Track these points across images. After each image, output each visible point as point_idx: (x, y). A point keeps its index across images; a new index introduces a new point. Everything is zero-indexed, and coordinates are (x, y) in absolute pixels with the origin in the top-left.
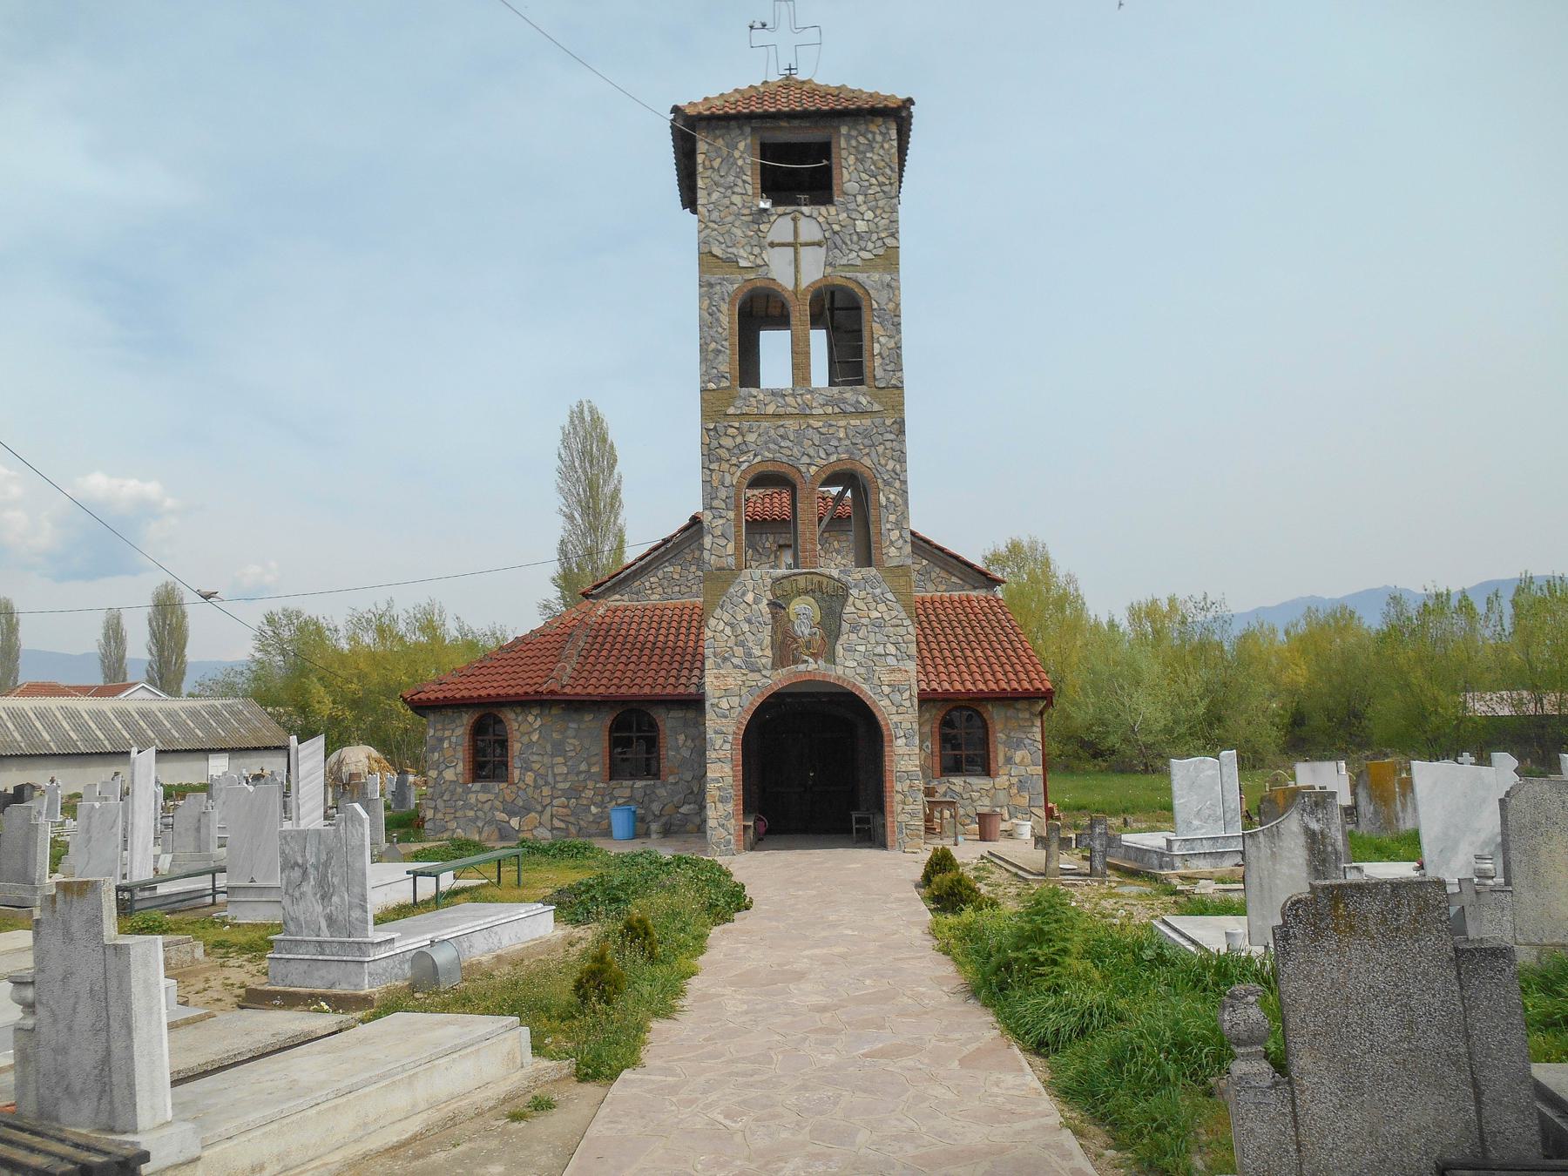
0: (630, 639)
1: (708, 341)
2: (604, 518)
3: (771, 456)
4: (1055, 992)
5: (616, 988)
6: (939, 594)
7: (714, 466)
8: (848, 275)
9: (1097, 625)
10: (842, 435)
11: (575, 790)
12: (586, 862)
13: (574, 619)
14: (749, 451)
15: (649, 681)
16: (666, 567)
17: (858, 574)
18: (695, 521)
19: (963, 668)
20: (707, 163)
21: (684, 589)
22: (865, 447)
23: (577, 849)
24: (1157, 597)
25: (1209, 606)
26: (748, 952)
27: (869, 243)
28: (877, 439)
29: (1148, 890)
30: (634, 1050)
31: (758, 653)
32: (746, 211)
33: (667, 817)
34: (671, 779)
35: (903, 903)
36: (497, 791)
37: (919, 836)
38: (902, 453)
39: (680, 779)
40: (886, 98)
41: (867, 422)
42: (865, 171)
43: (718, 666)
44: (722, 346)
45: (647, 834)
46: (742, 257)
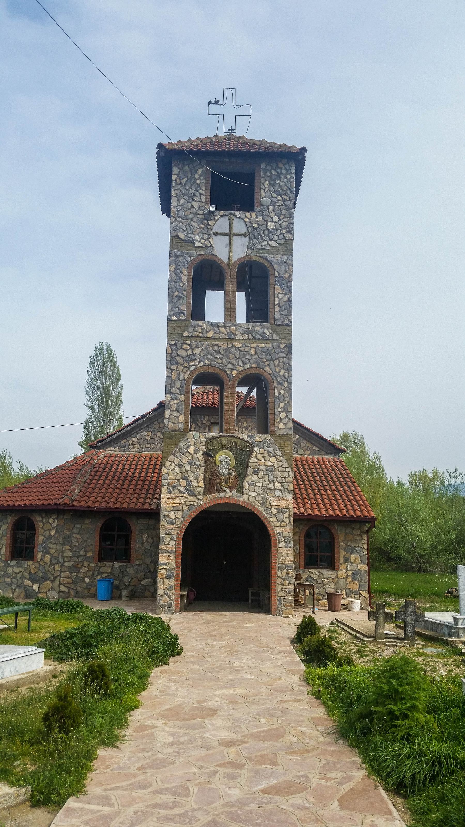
0: (118, 474)
1: (174, 291)
2: (112, 409)
3: (209, 363)
4: (408, 741)
5: (74, 721)
6: (306, 456)
7: (174, 367)
8: (262, 255)
9: (391, 483)
10: (253, 352)
11: (76, 567)
12: (77, 616)
13: (84, 461)
14: (196, 359)
15: (127, 500)
16: (142, 432)
17: (259, 438)
18: (161, 405)
19: (320, 501)
20: (178, 180)
21: (152, 446)
22: (267, 360)
23: (72, 606)
24: (426, 469)
25: (458, 476)
26: (177, 689)
27: (275, 236)
28: (275, 356)
29: (444, 651)
30: (81, 778)
31: (194, 484)
32: (201, 212)
33: (133, 587)
34: (137, 562)
35: (284, 655)
36: (26, 566)
37: (291, 607)
38: (290, 365)
39: (143, 563)
40: (290, 147)
41: (269, 345)
42: (275, 192)
43: (170, 492)
44: (182, 294)
45: (120, 597)
46: (197, 240)
